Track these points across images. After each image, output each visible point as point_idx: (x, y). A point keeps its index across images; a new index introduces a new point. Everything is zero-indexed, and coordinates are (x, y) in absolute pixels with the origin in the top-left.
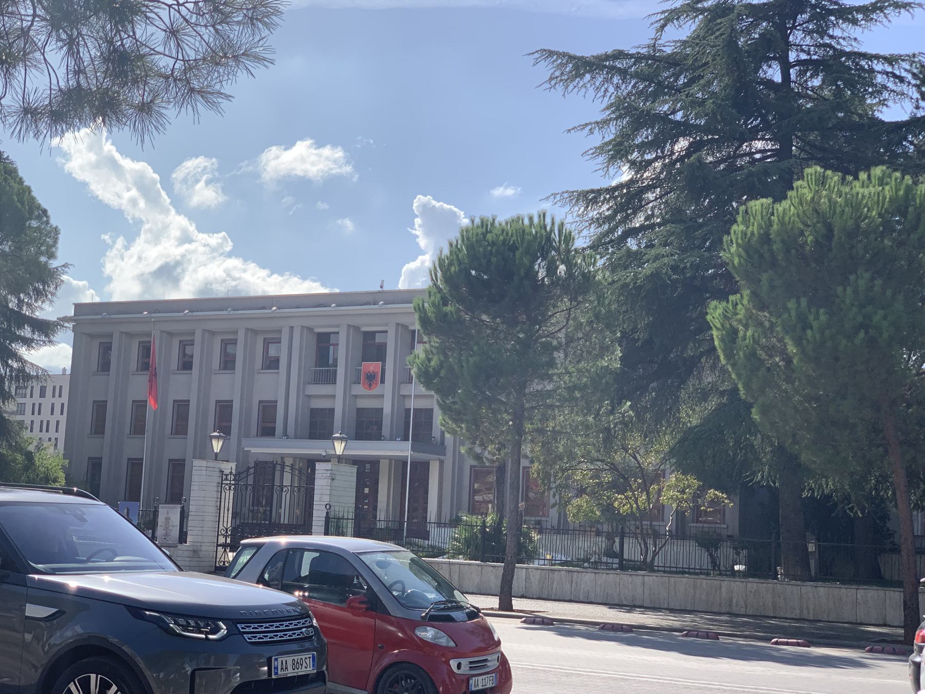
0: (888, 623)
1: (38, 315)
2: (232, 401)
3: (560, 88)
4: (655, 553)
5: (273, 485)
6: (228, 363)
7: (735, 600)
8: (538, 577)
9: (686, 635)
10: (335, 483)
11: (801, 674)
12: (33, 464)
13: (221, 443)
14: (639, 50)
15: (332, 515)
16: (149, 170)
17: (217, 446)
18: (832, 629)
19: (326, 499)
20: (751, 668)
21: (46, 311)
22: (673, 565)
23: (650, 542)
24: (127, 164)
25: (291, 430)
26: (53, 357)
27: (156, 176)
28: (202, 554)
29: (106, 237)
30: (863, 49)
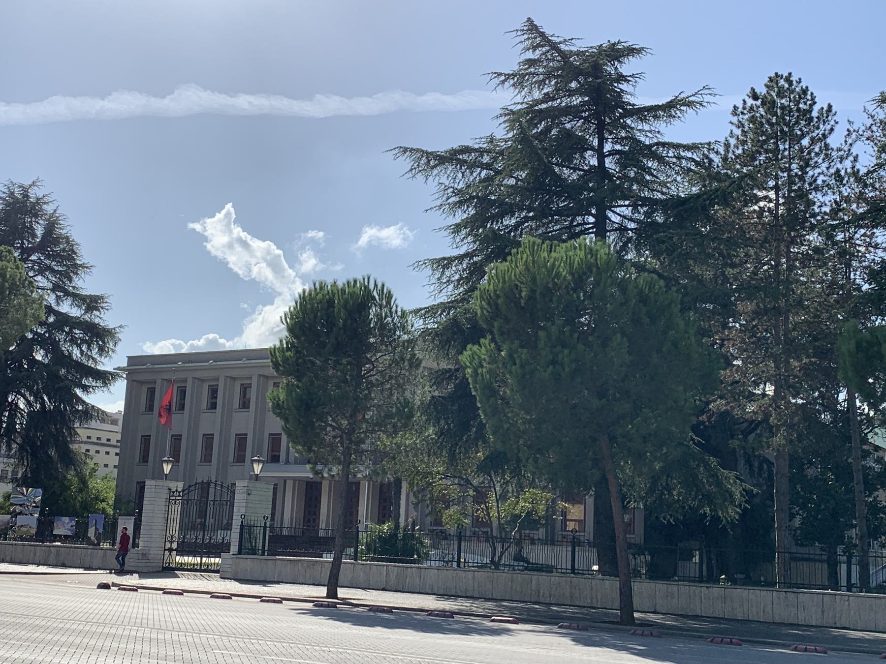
0: (658, 610)
1: (100, 367)
2: (246, 435)
3: (420, 177)
4: (502, 553)
5: (208, 499)
6: (245, 404)
7: (541, 592)
8: (395, 573)
9: (429, 615)
10: (251, 497)
11: (368, 633)
12: (88, 487)
13: (170, 466)
14: (481, 145)
15: (245, 523)
16: (273, 247)
17: (167, 468)
18: (606, 615)
19: (243, 511)
20: (446, 642)
21: (106, 365)
22: (564, 567)
23: (499, 547)
24: (257, 245)
25: (292, 459)
26: (110, 400)
27: (280, 252)
28: (150, 557)
29: (246, 306)
30: (666, 139)
